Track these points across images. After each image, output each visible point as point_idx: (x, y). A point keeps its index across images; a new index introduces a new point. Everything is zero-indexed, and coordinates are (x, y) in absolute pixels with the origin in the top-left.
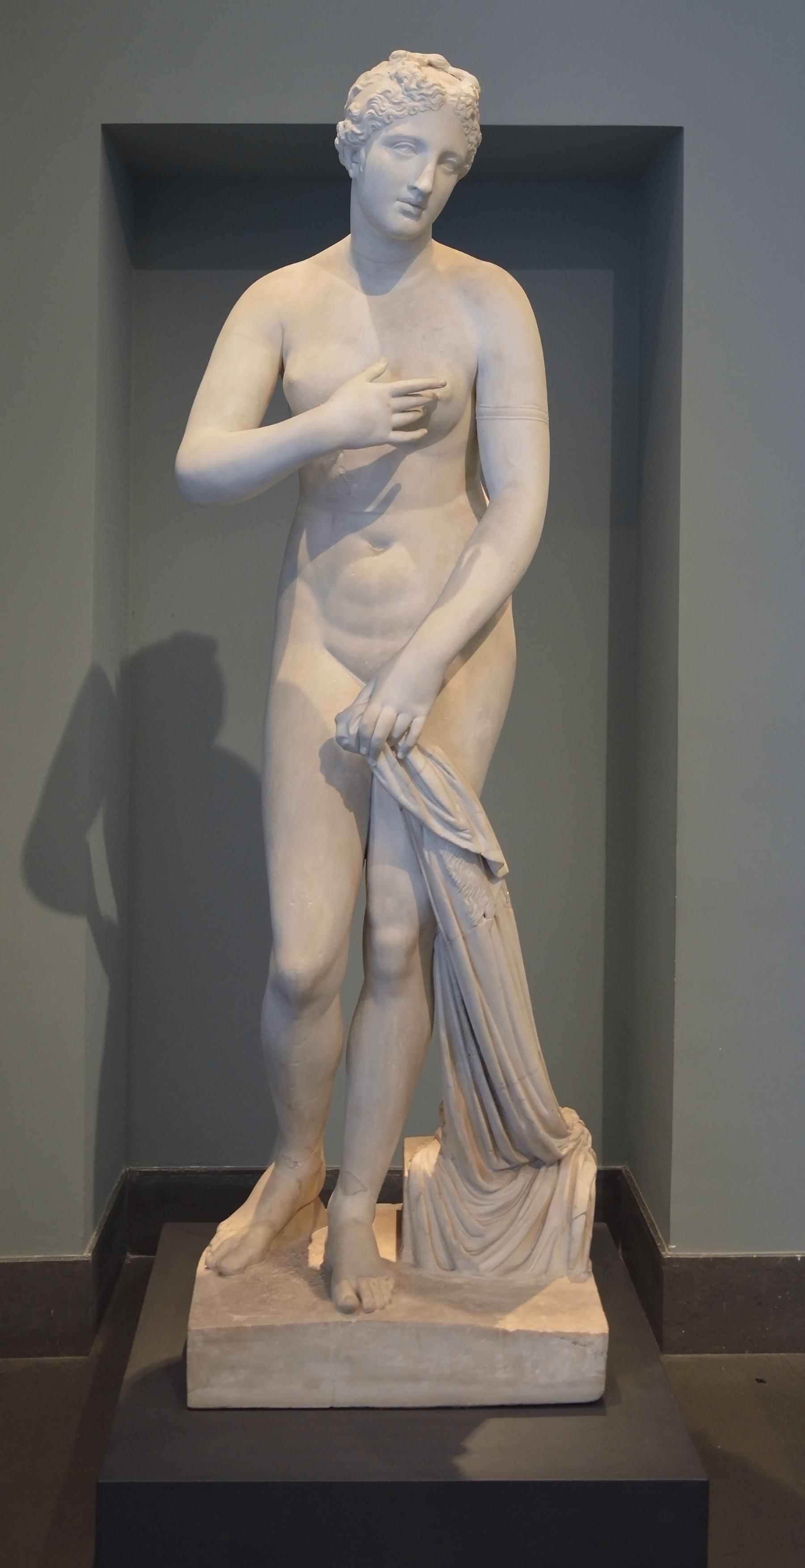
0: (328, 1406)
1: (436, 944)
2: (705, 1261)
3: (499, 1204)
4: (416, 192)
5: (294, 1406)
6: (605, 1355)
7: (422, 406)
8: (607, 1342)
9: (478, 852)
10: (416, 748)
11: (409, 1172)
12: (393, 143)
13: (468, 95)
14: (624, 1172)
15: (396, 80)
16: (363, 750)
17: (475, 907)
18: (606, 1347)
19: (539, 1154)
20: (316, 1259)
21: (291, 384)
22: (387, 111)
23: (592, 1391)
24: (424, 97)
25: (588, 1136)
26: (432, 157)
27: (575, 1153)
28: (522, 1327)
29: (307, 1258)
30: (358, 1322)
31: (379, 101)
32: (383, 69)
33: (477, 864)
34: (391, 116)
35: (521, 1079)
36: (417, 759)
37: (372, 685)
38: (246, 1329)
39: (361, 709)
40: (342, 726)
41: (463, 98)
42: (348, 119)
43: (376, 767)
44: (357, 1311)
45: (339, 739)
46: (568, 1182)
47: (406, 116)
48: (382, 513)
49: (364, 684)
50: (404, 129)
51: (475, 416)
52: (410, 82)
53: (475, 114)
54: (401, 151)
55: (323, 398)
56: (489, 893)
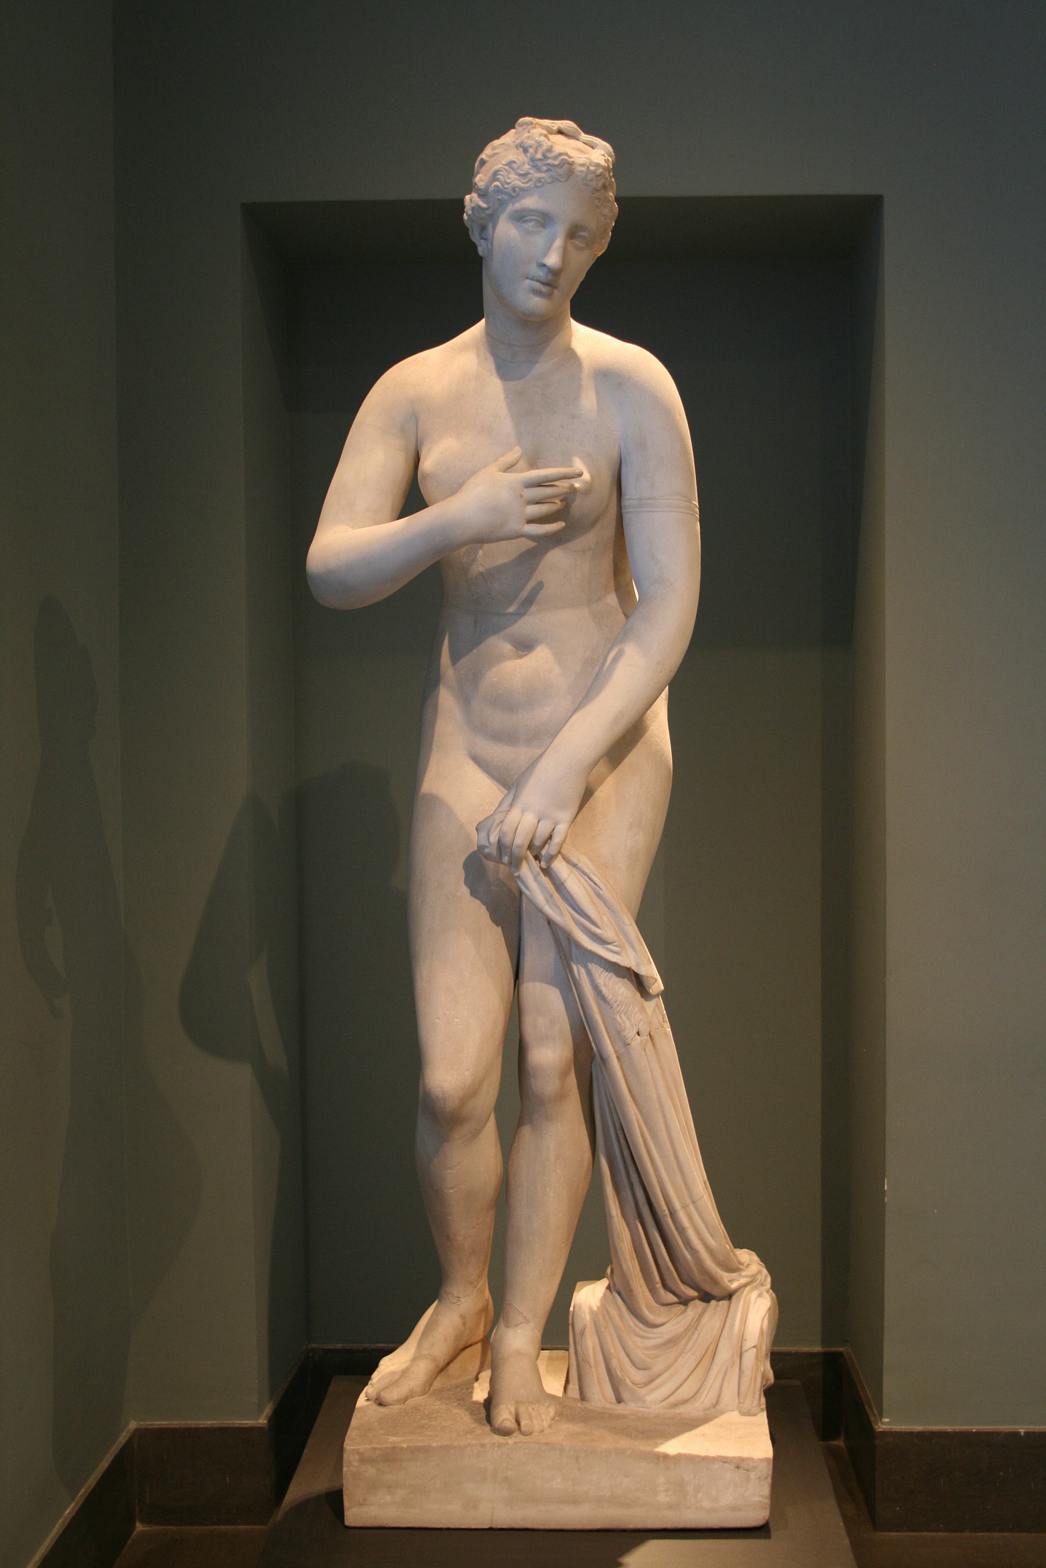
0: (487, 1527)
1: (593, 1067)
2: (921, 1435)
3: (667, 1337)
4: (545, 270)
5: (452, 1526)
6: (769, 1480)
7: (561, 498)
8: (771, 1467)
9: (628, 966)
10: (560, 856)
11: (574, 1307)
12: (520, 217)
13: (598, 165)
14: (845, 1354)
15: (521, 149)
16: (506, 859)
17: (628, 1024)
18: (771, 1472)
19: (708, 1288)
20: (480, 1394)
21: (425, 477)
22: (512, 184)
23: (756, 1516)
24: (551, 168)
25: (766, 1277)
26: (560, 232)
27: (747, 1289)
28: (683, 1451)
29: (472, 1393)
30: (515, 1443)
31: (504, 173)
32: (509, 138)
33: (628, 980)
34: (516, 189)
35: (685, 1207)
36: (560, 867)
37: (513, 792)
38: (402, 1449)
39: (498, 818)
40: (483, 834)
41: (592, 168)
42: (475, 193)
43: (519, 877)
44: (514, 1435)
45: (481, 848)
46: (739, 1316)
47: (533, 188)
48: (524, 614)
49: (507, 792)
50: (530, 202)
51: (621, 509)
52: (536, 152)
53: (607, 184)
54: (530, 226)
55: (454, 489)
56: (643, 1009)
